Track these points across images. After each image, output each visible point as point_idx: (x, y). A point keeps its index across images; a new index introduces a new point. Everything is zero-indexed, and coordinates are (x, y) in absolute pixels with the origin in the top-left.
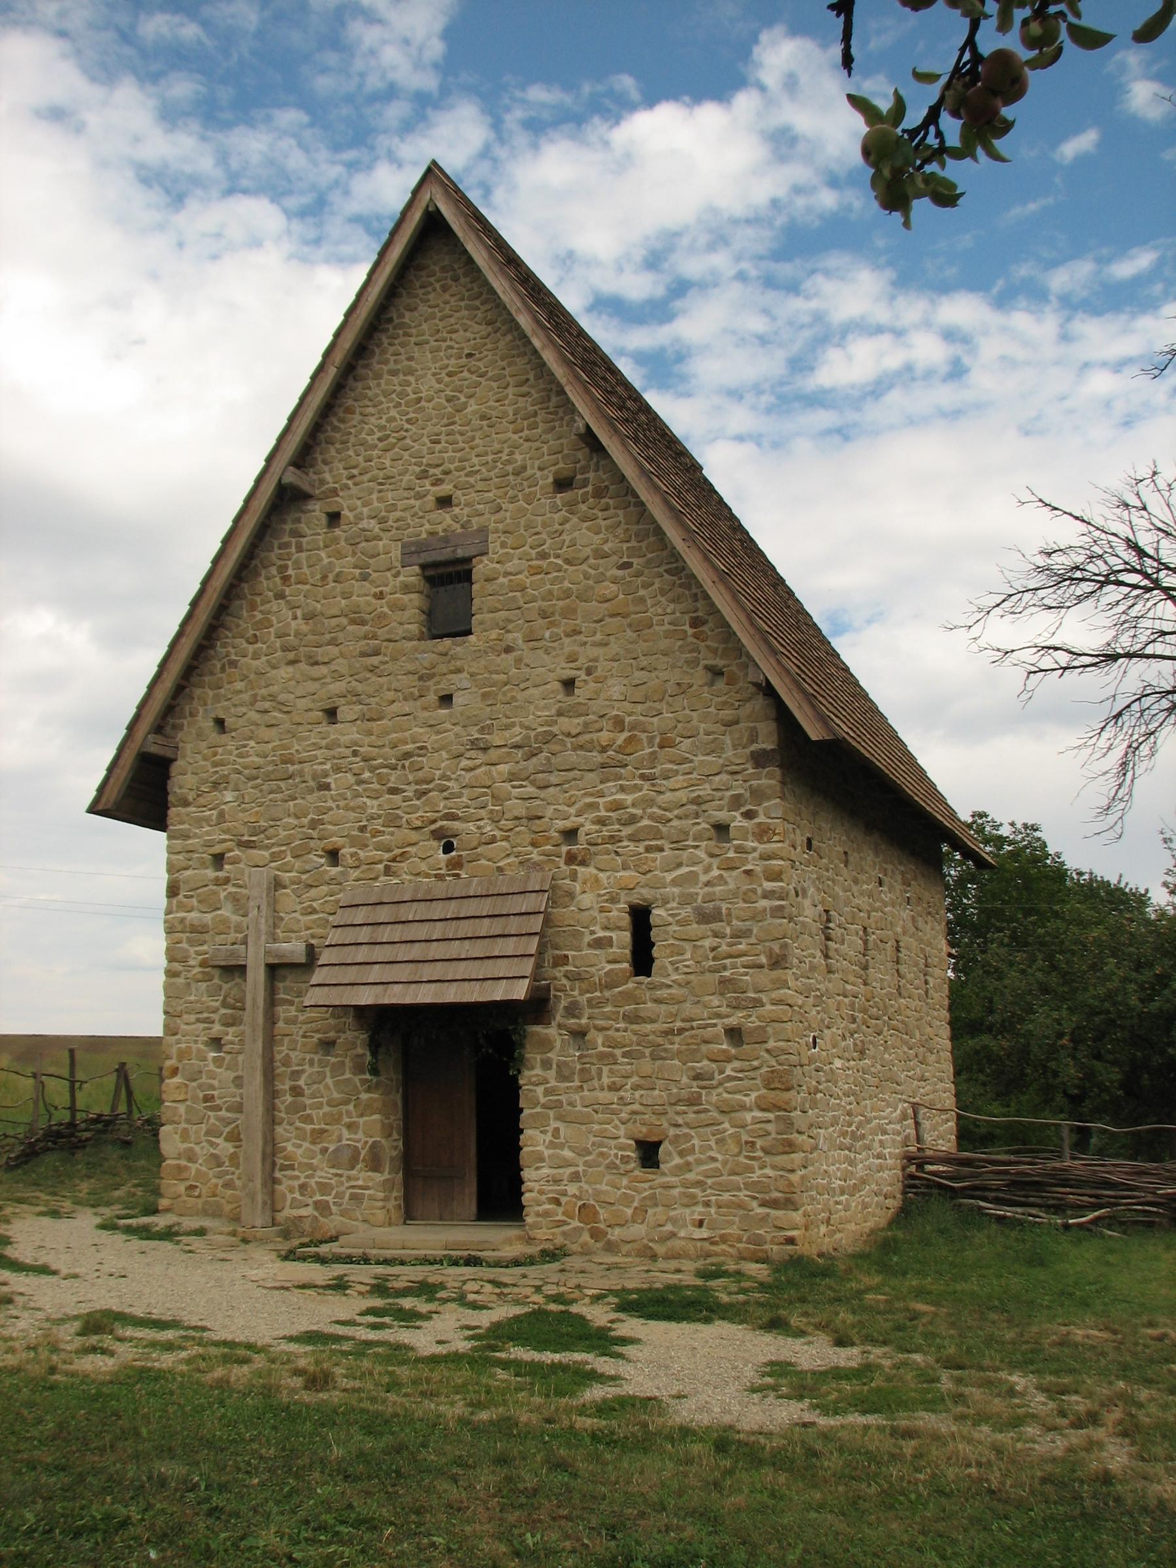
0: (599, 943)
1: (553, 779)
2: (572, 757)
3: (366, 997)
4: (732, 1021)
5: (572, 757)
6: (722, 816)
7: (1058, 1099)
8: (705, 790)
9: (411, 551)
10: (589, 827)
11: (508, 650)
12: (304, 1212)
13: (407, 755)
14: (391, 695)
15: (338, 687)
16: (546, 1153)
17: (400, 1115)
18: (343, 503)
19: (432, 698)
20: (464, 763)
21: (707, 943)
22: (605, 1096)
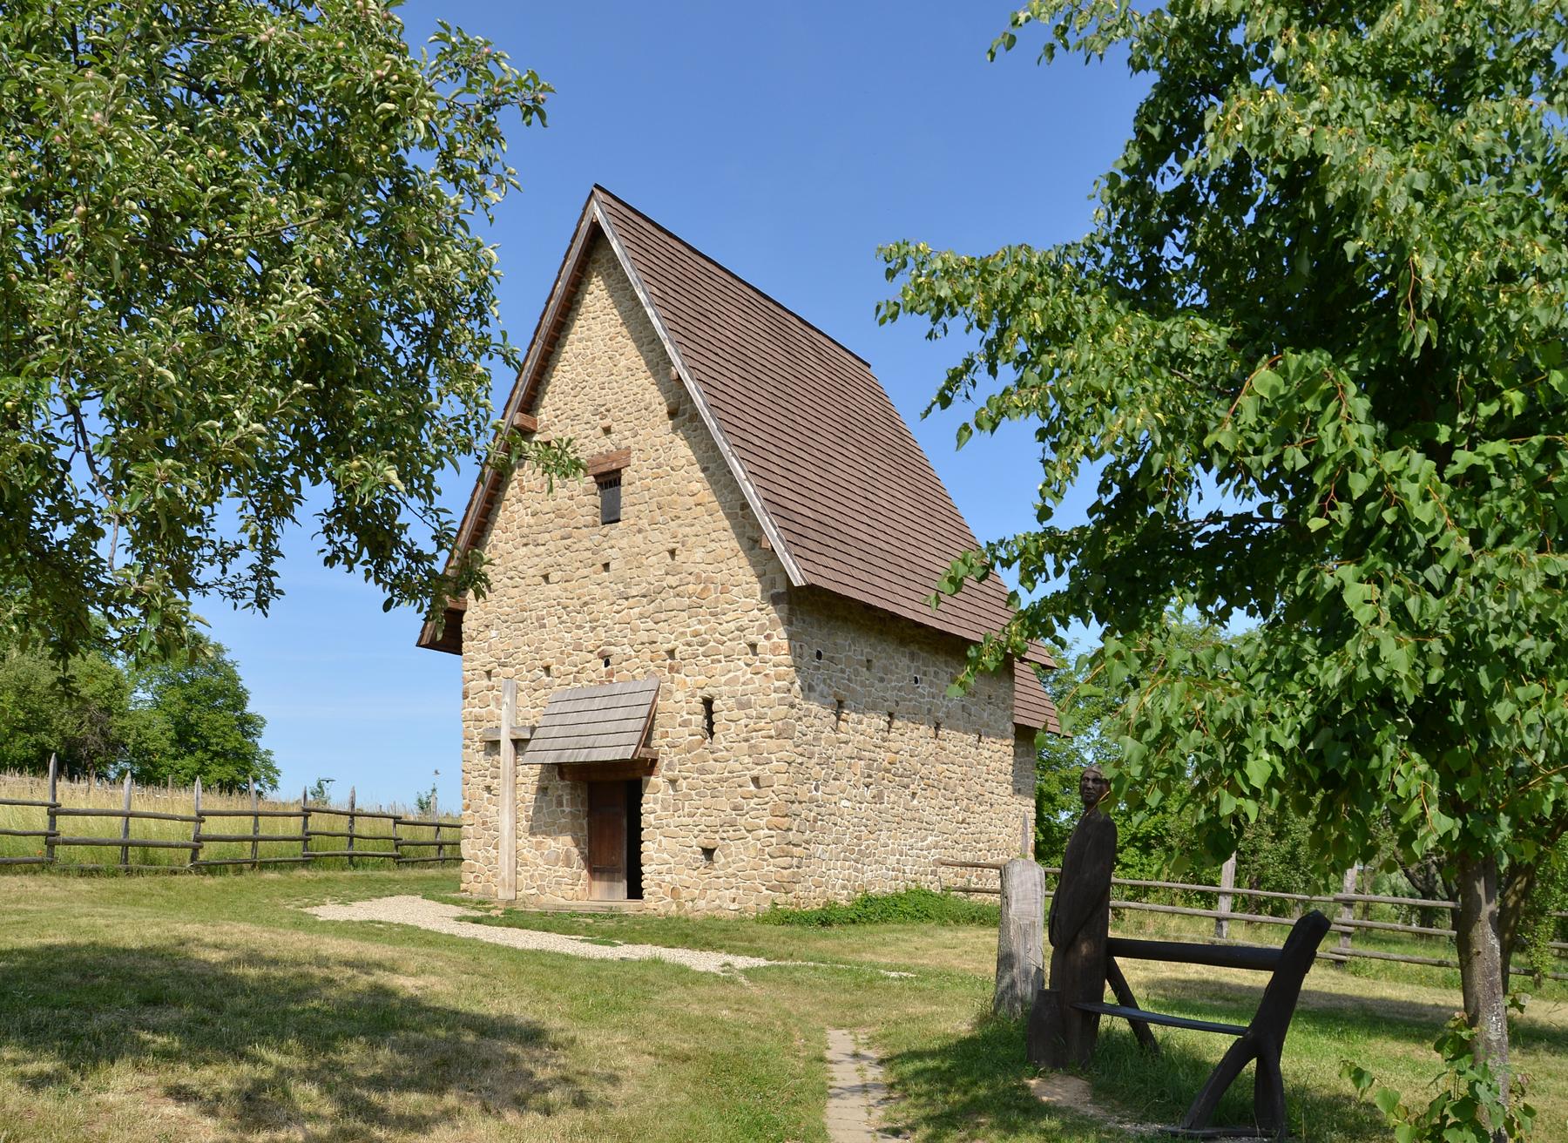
0: (685, 724)
1: (663, 616)
2: (674, 602)
3: (568, 757)
4: (755, 773)
5: (674, 602)
6: (753, 638)
8: (745, 622)
10: (681, 648)
11: (640, 531)
13: (586, 604)
19: (599, 566)
20: (616, 607)
21: (743, 722)
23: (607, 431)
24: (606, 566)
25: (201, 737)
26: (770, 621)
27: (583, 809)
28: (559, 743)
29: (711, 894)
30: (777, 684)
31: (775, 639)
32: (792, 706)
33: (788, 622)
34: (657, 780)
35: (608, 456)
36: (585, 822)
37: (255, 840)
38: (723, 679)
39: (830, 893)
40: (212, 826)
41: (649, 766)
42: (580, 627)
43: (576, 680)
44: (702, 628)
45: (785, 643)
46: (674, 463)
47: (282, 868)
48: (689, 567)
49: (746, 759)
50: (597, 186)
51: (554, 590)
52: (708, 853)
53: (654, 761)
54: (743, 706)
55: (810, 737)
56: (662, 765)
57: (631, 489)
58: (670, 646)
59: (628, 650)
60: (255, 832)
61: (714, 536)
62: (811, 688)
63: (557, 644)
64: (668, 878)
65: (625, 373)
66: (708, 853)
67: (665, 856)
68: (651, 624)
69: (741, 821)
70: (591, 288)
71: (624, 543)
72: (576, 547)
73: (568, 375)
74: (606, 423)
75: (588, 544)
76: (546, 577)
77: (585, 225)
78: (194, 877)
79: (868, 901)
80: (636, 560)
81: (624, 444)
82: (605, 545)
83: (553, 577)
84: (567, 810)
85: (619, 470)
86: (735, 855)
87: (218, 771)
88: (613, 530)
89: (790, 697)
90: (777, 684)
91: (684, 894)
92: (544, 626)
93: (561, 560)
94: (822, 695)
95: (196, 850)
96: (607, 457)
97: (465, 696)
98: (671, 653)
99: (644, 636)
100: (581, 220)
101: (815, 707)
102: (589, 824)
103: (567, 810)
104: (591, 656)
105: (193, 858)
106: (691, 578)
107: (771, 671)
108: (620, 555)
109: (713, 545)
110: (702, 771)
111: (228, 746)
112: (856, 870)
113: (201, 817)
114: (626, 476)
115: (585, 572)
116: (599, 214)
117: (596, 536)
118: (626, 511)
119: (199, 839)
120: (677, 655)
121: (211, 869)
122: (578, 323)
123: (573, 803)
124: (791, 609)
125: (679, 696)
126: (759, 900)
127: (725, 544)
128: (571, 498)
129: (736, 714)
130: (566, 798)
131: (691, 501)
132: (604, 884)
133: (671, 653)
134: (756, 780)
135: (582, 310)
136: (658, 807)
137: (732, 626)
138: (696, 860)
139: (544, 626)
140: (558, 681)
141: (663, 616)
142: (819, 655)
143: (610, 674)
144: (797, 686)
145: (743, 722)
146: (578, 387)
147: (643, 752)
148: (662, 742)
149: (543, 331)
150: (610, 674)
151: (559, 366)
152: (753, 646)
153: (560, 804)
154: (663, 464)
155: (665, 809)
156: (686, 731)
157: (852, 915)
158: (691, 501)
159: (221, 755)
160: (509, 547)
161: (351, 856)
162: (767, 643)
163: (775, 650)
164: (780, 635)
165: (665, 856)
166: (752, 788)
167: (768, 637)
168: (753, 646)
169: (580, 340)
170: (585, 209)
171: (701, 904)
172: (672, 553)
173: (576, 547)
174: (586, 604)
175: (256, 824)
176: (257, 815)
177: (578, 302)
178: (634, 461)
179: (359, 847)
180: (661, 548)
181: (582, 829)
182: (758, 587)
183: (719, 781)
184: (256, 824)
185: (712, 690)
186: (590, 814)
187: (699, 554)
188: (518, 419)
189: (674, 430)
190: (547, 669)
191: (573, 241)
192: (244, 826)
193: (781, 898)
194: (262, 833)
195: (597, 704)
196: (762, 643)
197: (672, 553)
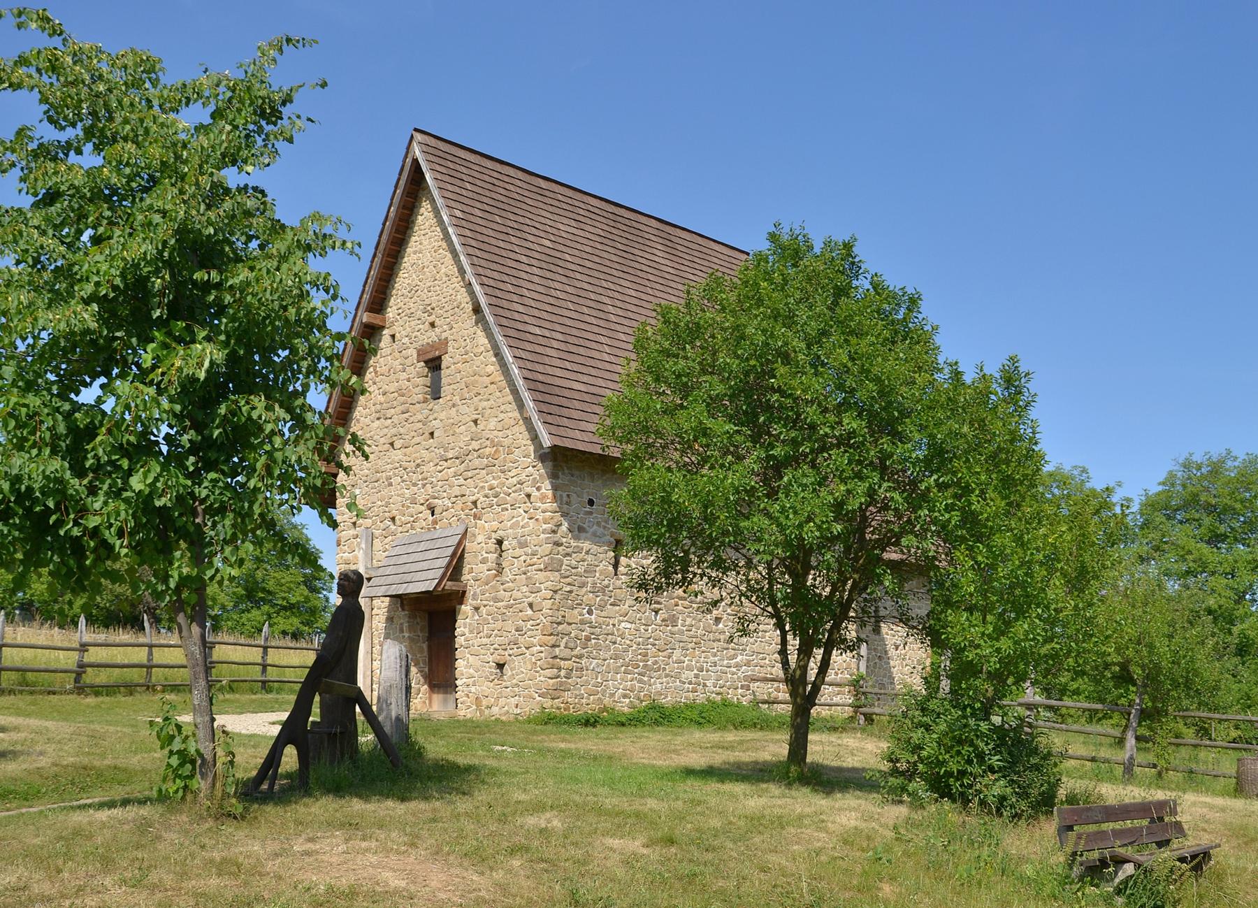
0: (484, 561)
1: (470, 474)
2: (477, 462)
3: (402, 590)
4: (530, 600)
5: (477, 462)
6: (529, 490)
7: (1056, 740)
8: (523, 477)
9: (420, 353)
10: (482, 499)
11: (454, 405)
12: (91, 446)
13: (418, 465)
14: (413, 434)
15: (394, 431)
16: (465, 666)
17: (426, 654)
18: (396, 329)
19: (427, 434)
20: (439, 468)
21: (522, 558)
22: (485, 640)
23: (432, 325)
24: (432, 434)
25: (269, 593)
26: (540, 475)
27: (423, 635)
28: (390, 580)
29: (502, 701)
30: (545, 526)
31: (543, 490)
32: (558, 544)
33: (553, 476)
34: (466, 609)
35: (432, 346)
36: (425, 646)
37: (149, 667)
38: (509, 524)
39: (607, 701)
40: (94, 655)
41: (460, 597)
42: (415, 485)
43: (412, 528)
44: (495, 483)
45: (550, 493)
46: (476, 350)
47: (179, 691)
48: (487, 434)
49: (525, 589)
50: (416, 130)
51: (397, 455)
52: (500, 666)
53: (464, 592)
54: (523, 545)
55: (581, 570)
56: (469, 595)
57: (448, 371)
58: (474, 498)
59: (446, 502)
60: (149, 660)
61: (503, 407)
62: (581, 529)
63: (399, 499)
64: (473, 689)
65: (445, 279)
66: (500, 666)
67: (471, 671)
68: (462, 481)
69: (521, 639)
70: (422, 210)
71: (443, 415)
72: (411, 419)
73: (407, 281)
74: (431, 319)
75: (420, 417)
76: (392, 444)
77: (409, 160)
78: (75, 696)
79: (654, 707)
80: (451, 428)
81: (444, 335)
82: (431, 418)
83: (397, 445)
84: (407, 635)
85: (439, 358)
86: (519, 668)
87: (284, 623)
88: (437, 405)
89: (557, 537)
90: (545, 526)
91: (485, 702)
92: (390, 484)
93: (402, 431)
94: (594, 534)
95: (79, 676)
96: (432, 346)
97: (339, 545)
98: (475, 503)
99: (456, 491)
100: (406, 157)
101: (586, 545)
102: (429, 647)
103: (407, 635)
104: (423, 508)
105: (77, 680)
106: (488, 443)
107: (540, 516)
108: (441, 425)
109: (502, 416)
110: (496, 600)
111: (293, 600)
112: (640, 681)
113: (84, 647)
114: (446, 361)
115: (417, 440)
116: (418, 153)
117: (421, 412)
118: (446, 390)
119: (82, 666)
120: (479, 506)
121: (97, 690)
122: (413, 239)
123: (411, 629)
124: (555, 466)
125: (480, 538)
126: (531, 705)
127: (510, 415)
128: (409, 380)
129: (518, 552)
130: (406, 625)
131: (487, 380)
132: (441, 696)
133: (475, 503)
134: (531, 605)
135: (416, 228)
136: (466, 631)
137: (515, 480)
138: (491, 674)
139: (390, 484)
140: (400, 529)
141: (470, 474)
142: (591, 502)
143: (435, 522)
144: (565, 527)
145: (522, 558)
146: (414, 290)
147: (449, 585)
148: (468, 577)
149: (382, 247)
150: (435, 522)
151: (401, 274)
152: (529, 496)
153: (402, 631)
154: (472, 353)
155: (471, 632)
156: (485, 567)
157: (623, 720)
158: (487, 380)
159: (290, 608)
160: (367, 421)
161: (264, 682)
162: (537, 494)
163: (543, 499)
164: (546, 486)
165: (471, 671)
166: (530, 612)
167: (538, 489)
168: (529, 496)
169: (415, 253)
170: (408, 148)
171: (495, 710)
172: (475, 422)
173: (411, 419)
174: (418, 465)
175: (150, 654)
176: (151, 646)
177: (413, 222)
178: (450, 349)
179: (272, 674)
180: (468, 419)
181: (421, 651)
182: (532, 448)
183: (507, 607)
184: (150, 654)
185: (500, 533)
186: (430, 639)
187: (493, 423)
188: (366, 317)
189: (477, 323)
190: (393, 519)
191: (400, 174)
192: (140, 655)
193: (548, 703)
194: (155, 661)
195: (423, 546)
196: (535, 494)
197: (475, 422)
